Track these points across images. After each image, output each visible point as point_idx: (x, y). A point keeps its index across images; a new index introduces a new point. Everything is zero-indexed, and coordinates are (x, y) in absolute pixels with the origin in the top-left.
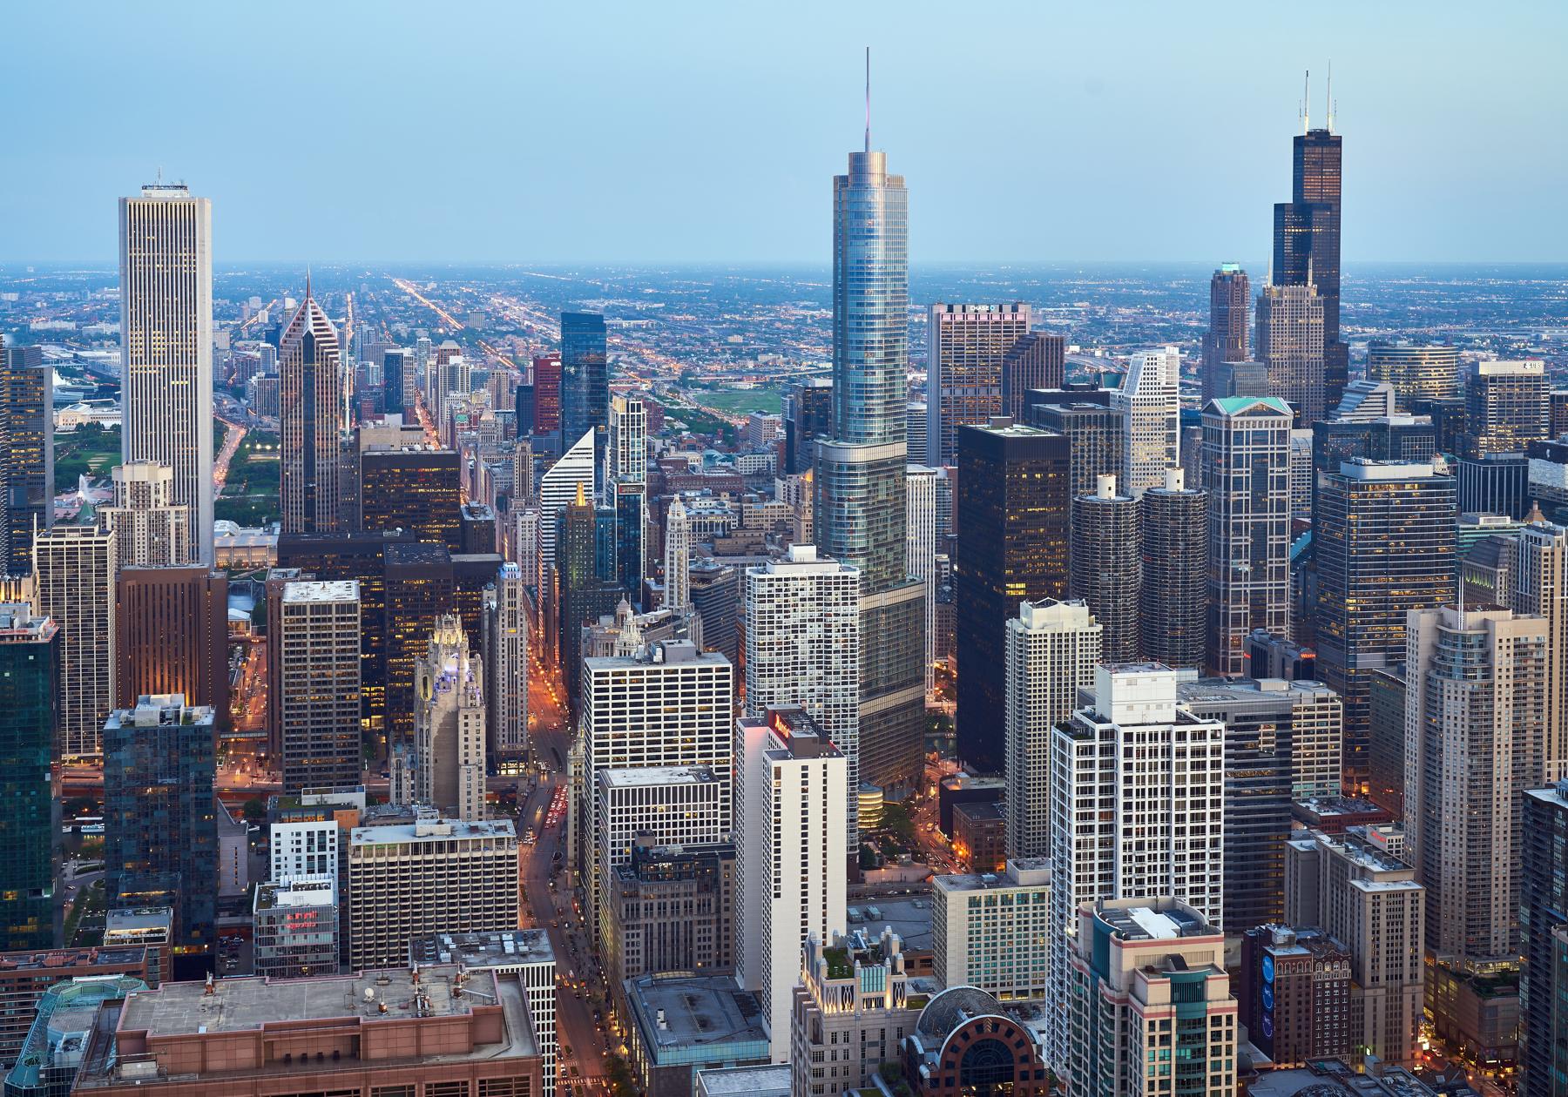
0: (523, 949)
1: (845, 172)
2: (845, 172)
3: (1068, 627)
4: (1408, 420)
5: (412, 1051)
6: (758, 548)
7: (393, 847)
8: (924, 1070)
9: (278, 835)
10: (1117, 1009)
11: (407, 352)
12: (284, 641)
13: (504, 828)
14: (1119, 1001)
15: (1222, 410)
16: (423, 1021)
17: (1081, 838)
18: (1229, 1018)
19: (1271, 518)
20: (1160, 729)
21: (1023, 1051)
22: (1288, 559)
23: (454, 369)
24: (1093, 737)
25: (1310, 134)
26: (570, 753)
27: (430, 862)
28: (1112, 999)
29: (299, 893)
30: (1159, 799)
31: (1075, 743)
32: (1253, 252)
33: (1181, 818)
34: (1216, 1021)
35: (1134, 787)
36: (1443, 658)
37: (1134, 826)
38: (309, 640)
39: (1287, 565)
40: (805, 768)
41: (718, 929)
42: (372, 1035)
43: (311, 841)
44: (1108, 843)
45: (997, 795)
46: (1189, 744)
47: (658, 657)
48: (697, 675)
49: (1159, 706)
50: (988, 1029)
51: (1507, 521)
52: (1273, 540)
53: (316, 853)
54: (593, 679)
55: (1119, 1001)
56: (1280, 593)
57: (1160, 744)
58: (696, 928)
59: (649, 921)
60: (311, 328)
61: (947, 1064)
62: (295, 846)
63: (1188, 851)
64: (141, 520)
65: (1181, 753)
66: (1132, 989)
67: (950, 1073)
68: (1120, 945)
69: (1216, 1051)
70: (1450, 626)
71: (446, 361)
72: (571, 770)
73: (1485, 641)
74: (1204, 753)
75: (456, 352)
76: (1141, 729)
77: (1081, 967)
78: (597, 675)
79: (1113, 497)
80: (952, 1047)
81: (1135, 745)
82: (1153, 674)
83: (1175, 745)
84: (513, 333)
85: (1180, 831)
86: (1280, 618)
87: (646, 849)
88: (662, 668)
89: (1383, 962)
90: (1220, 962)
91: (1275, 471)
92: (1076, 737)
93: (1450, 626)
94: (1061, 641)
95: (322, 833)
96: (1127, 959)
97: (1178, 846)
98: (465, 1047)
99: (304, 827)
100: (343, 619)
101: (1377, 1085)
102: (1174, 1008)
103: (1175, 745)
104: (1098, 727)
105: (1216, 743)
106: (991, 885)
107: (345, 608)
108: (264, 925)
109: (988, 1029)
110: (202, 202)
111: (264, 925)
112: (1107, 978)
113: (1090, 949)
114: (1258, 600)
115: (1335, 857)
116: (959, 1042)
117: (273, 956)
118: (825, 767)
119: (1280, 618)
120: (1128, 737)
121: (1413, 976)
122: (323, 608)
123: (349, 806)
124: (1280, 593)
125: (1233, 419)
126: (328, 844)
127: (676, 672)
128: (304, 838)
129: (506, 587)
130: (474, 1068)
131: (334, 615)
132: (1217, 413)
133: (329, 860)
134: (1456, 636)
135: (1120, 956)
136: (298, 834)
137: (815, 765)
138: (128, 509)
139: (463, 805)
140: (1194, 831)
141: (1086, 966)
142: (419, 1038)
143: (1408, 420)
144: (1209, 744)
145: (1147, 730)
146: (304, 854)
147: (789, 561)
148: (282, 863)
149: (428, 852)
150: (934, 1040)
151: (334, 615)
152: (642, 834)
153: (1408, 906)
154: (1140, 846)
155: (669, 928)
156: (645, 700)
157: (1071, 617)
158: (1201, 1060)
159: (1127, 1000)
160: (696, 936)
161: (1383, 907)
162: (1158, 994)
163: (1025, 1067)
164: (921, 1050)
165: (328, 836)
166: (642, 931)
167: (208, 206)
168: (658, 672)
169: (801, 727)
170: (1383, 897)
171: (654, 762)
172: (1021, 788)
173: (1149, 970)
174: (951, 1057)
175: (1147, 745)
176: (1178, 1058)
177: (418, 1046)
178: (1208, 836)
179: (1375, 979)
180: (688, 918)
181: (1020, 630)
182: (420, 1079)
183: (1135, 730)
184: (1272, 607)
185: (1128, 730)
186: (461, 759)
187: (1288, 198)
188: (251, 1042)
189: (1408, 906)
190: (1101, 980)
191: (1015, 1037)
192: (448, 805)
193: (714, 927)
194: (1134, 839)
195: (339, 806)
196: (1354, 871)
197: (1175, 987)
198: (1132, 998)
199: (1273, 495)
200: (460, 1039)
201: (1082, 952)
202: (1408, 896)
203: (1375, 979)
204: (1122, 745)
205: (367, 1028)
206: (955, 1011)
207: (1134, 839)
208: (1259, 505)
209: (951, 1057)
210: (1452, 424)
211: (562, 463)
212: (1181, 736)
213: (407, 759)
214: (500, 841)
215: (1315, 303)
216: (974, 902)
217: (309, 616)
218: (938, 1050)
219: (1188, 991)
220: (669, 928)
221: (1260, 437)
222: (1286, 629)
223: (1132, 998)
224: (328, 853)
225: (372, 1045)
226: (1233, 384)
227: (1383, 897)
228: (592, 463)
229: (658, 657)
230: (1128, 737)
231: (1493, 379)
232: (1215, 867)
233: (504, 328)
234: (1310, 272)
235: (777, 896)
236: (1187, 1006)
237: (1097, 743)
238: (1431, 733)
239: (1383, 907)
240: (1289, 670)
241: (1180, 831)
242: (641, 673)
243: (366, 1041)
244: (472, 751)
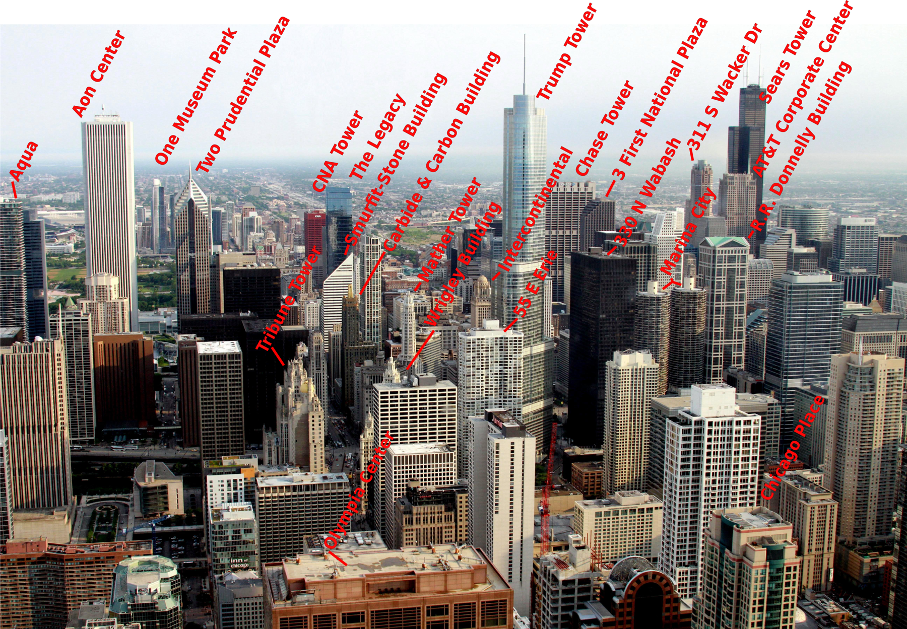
0: (368, 541)
1: (511, 106)
2: (511, 106)
3: (641, 365)
4: (804, 250)
5: (442, 588)
6: (444, 322)
7: (281, 488)
8: (616, 600)
9: (211, 482)
10: (736, 564)
11: (223, 210)
12: (200, 375)
13: (341, 477)
14: (738, 560)
15: (712, 244)
16: (446, 572)
17: (683, 478)
18: (795, 568)
19: (735, 304)
20: (726, 419)
21: (668, 588)
22: (744, 327)
23: (251, 220)
24: (690, 424)
25: (749, 87)
26: (361, 436)
27: (334, 494)
28: (734, 559)
29: (235, 512)
30: (725, 457)
31: (681, 428)
32: (716, 153)
33: (736, 467)
34: (789, 569)
35: (712, 450)
36: (849, 381)
37: (711, 471)
38: (214, 375)
39: (744, 330)
40: (513, 443)
41: (456, 531)
42: (422, 579)
43: (229, 485)
44: (696, 481)
45: (600, 458)
46: (742, 427)
47: (415, 383)
48: (399, 395)
49: (726, 407)
50: (650, 578)
51: (860, 306)
52: (736, 317)
53: (233, 492)
54: (380, 395)
55: (738, 560)
56: (740, 346)
57: (727, 427)
58: (444, 530)
59: (418, 527)
60: (192, 197)
61: (628, 596)
62: (221, 488)
63: (739, 484)
64: (101, 308)
65: (738, 432)
66: (745, 554)
67: (629, 601)
68: (739, 531)
69: (788, 584)
70: (854, 363)
71: (247, 215)
72: (363, 446)
73: (872, 371)
74: (750, 432)
75: (252, 210)
76: (717, 420)
77: (713, 544)
78: (382, 393)
79: (656, 293)
80: (631, 587)
81: (714, 428)
82: (723, 390)
83: (735, 428)
84: (278, 198)
85: (736, 474)
86: (739, 360)
87: (415, 488)
88: (418, 389)
89: (814, 542)
90: (789, 539)
91: (738, 278)
92: (682, 424)
93: (854, 363)
94: (636, 373)
95: (235, 481)
96: (743, 539)
97: (734, 482)
98: (470, 585)
99: (225, 477)
100: (233, 363)
101: (812, 604)
102: (768, 563)
103: (735, 428)
104: (694, 419)
105: (756, 426)
106: (607, 504)
107: (233, 356)
108: (217, 529)
109: (650, 578)
110: (129, 123)
111: (217, 529)
112: (730, 549)
113: (719, 533)
114: (727, 351)
115: (789, 488)
116: (635, 584)
117: (223, 546)
118: (513, 443)
119: (739, 360)
120: (710, 424)
121: (829, 548)
122: (221, 357)
123: (248, 466)
124: (740, 346)
125: (717, 249)
126: (239, 487)
127: (425, 391)
128: (225, 484)
129: (315, 344)
130: (479, 596)
131: (228, 360)
132: (708, 245)
133: (239, 495)
134: (857, 369)
135: (739, 538)
136: (222, 481)
137: (518, 441)
138: (95, 301)
139: (312, 464)
140: (743, 473)
141: (718, 544)
142: (446, 581)
143: (804, 250)
144: (752, 427)
145: (720, 420)
146: (226, 492)
147: (484, 329)
148: (214, 497)
149: (301, 490)
150: (620, 584)
151: (228, 360)
152: (412, 480)
153: (828, 512)
154: (714, 482)
155: (429, 531)
156: (389, 408)
157: (640, 359)
158: (779, 589)
159: (742, 560)
160: (444, 534)
161: (816, 513)
162: (760, 556)
163: (668, 597)
164: (613, 589)
165: (239, 482)
166: (414, 533)
167: (131, 124)
168: (416, 392)
169: (508, 421)
170: (816, 508)
171: (413, 441)
172: (613, 456)
173: (754, 544)
174: (631, 592)
175: (720, 428)
176: (769, 588)
177: (446, 586)
178: (750, 476)
179: (810, 550)
180: (440, 525)
181: (614, 367)
182: (451, 602)
183: (714, 420)
184: (735, 354)
185: (710, 420)
186: (311, 441)
187: (736, 124)
188: (360, 584)
189: (828, 512)
190: (727, 550)
191: (664, 581)
192: (304, 464)
193: (454, 530)
194: (711, 478)
195: (244, 467)
196: (800, 494)
197: (768, 552)
198: (745, 559)
199: (737, 291)
200: (467, 581)
201: (714, 536)
202: (829, 508)
203: (810, 550)
204: (707, 428)
205: (419, 576)
206: (629, 570)
207: (711, 478)
208: (730, 297)
209: (631, 592)
210: (828, 255)
211: (335, 273)
212: (738, 423)
213: (274, 440)
214: (340, 484)
215: (751, 183)
216: (598, 514)
217: (214, 361)
218: (623, 589)
219: (775, 554)
220: (429, 531)
221: (731, 259)
222: (743, 366)
223: (745, 559)
224: (238, 491)
225: (422, 584)
226: (707, 229)
227: (816, 508)
228: (351, 273)
229: (415, 383)
230: (710, 424)
231: (849, 228)
232: (752, 492)
233: (271, 196)
234: (749, 166)
235: (497, 512)
236: (775, 562)
237: (693, 427)
238: (841, 420)
239: (816, 513)
240: (749, 387)
241: (736, 474)
242: (406, 392)
243: (419, 583)
244: (317, 435)
